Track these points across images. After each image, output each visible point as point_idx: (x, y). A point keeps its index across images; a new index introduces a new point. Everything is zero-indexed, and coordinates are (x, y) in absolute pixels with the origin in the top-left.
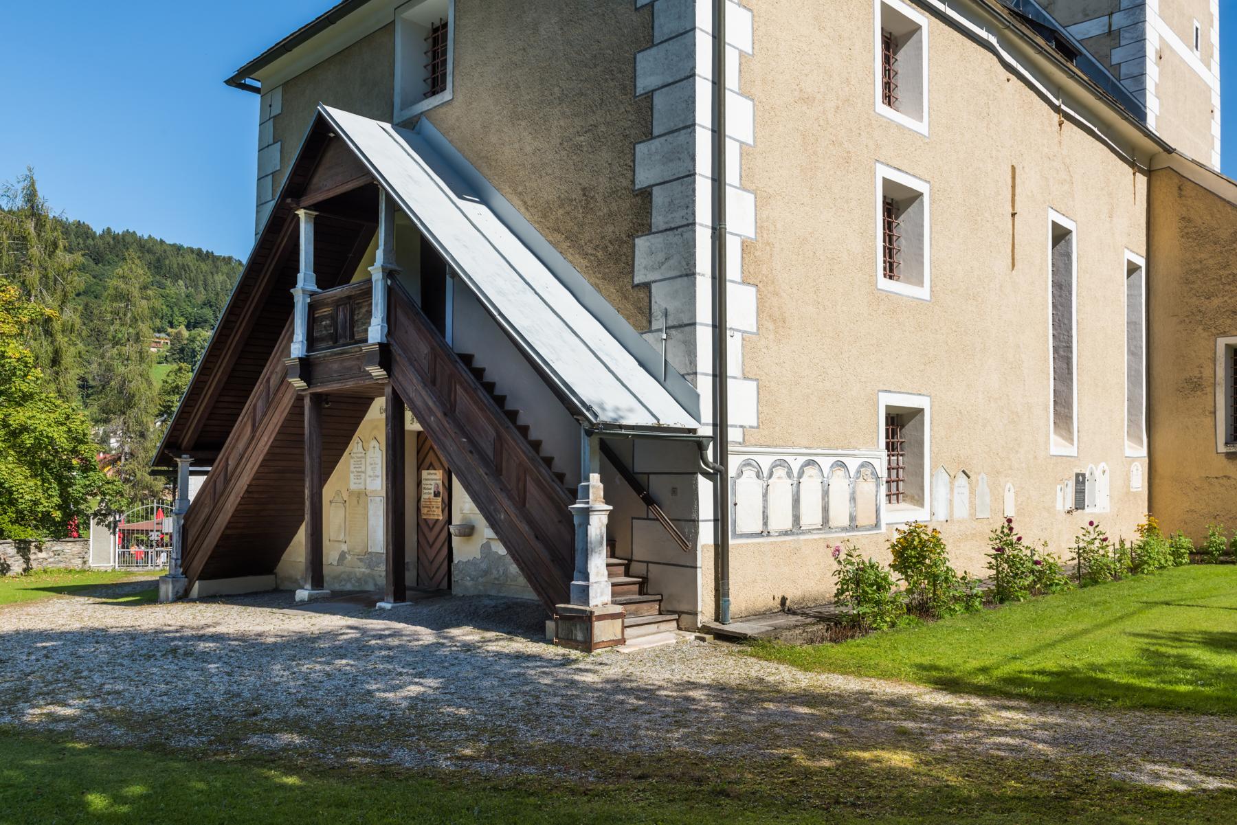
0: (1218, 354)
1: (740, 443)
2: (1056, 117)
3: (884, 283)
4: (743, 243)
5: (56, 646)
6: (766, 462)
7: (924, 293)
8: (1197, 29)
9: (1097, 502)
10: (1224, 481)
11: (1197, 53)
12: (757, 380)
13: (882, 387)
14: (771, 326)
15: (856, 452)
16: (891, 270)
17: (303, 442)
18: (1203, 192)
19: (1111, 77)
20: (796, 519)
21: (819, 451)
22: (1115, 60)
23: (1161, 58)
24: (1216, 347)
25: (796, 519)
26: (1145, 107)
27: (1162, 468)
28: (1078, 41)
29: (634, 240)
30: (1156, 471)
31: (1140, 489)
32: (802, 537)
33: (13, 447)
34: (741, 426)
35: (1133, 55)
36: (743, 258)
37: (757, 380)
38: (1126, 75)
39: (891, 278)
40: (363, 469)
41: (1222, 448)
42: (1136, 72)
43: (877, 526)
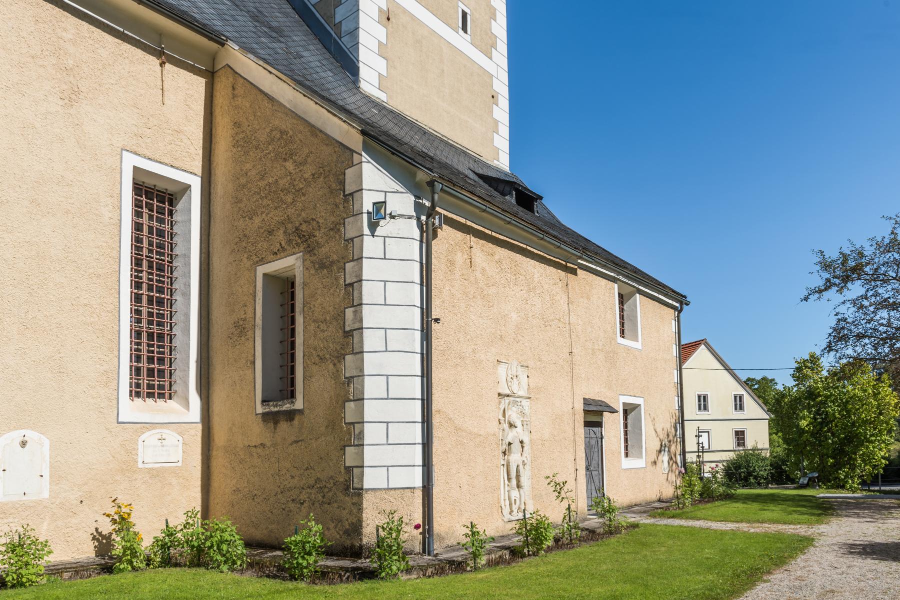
0: (257, 289)
3: (620, 340)
5: (327, 567)
7: (638, 345)
8: (464, 15)
10: (259, 450)
11: (467, 37)
16: (623, 334)
17: (882, 478)
18: (248, 85)
19: (334, 35)
22: (338, 19)
23: (388, 19)
24: (256, 278)
26: (358, 61)
27: (220, 437)
28: (312, 5)
29: (256, 267)
30: (213, 440)
31: (180, 464)
35: (351, 10)
38: (345, 31)
39: (623, 337)
41: (260, 409)
42: (352, 27)
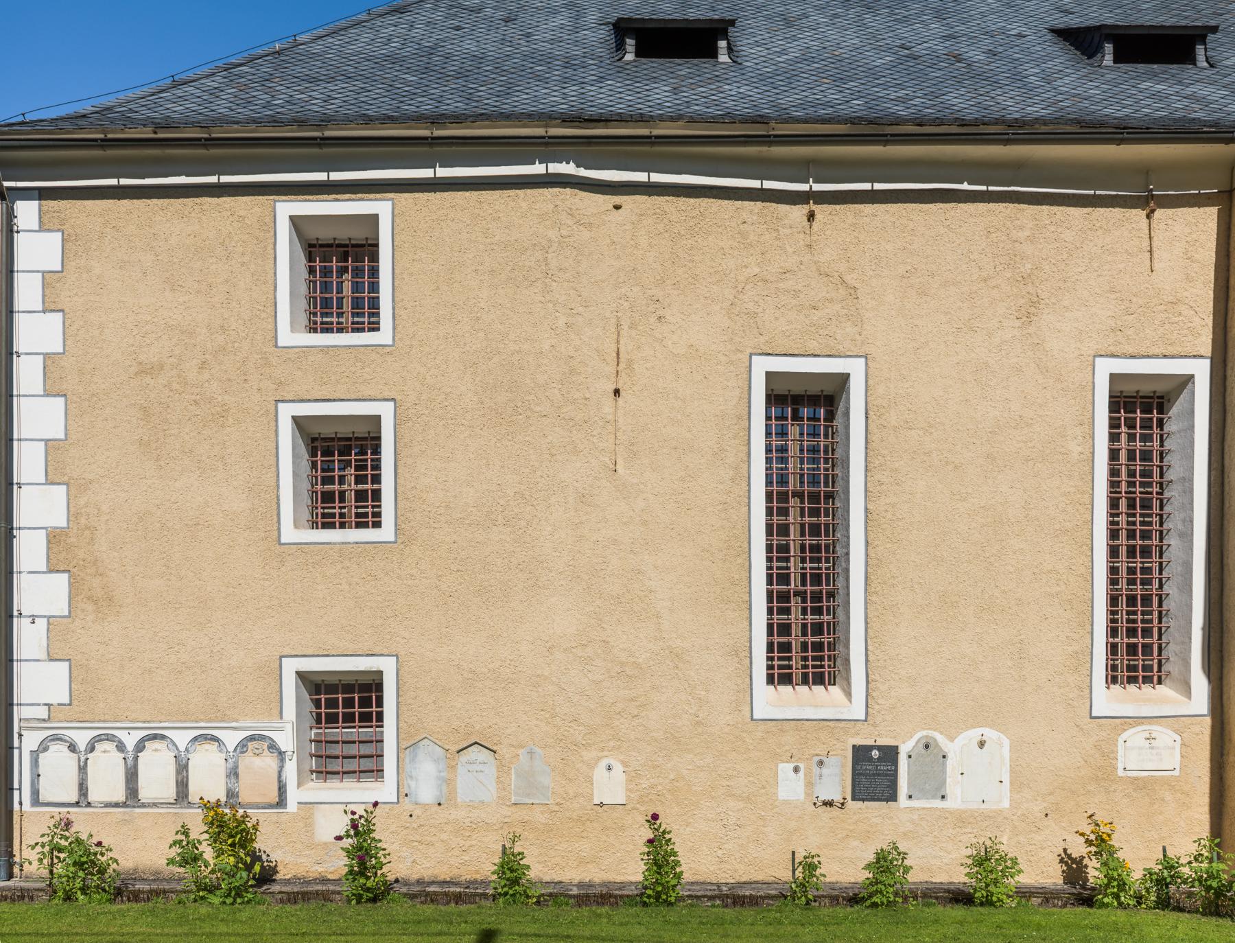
1: (44, 720)
2: (798, 213)
4: (48, 535)
6: (82, 738)
9: (949, 791)
12: (69, 660)
13: (287, 651)
14: (90, 607)
15: (234, 724)
20: (83, 789)
21: (166, 725)
25: (83, 789)
31: (1176, 773)
32: (138, 810)
33: (366, 868)
34: (46, 705)
36: (48, 549)
37: (69, 660)
40: (1120, 587)
43: (281, 802)
